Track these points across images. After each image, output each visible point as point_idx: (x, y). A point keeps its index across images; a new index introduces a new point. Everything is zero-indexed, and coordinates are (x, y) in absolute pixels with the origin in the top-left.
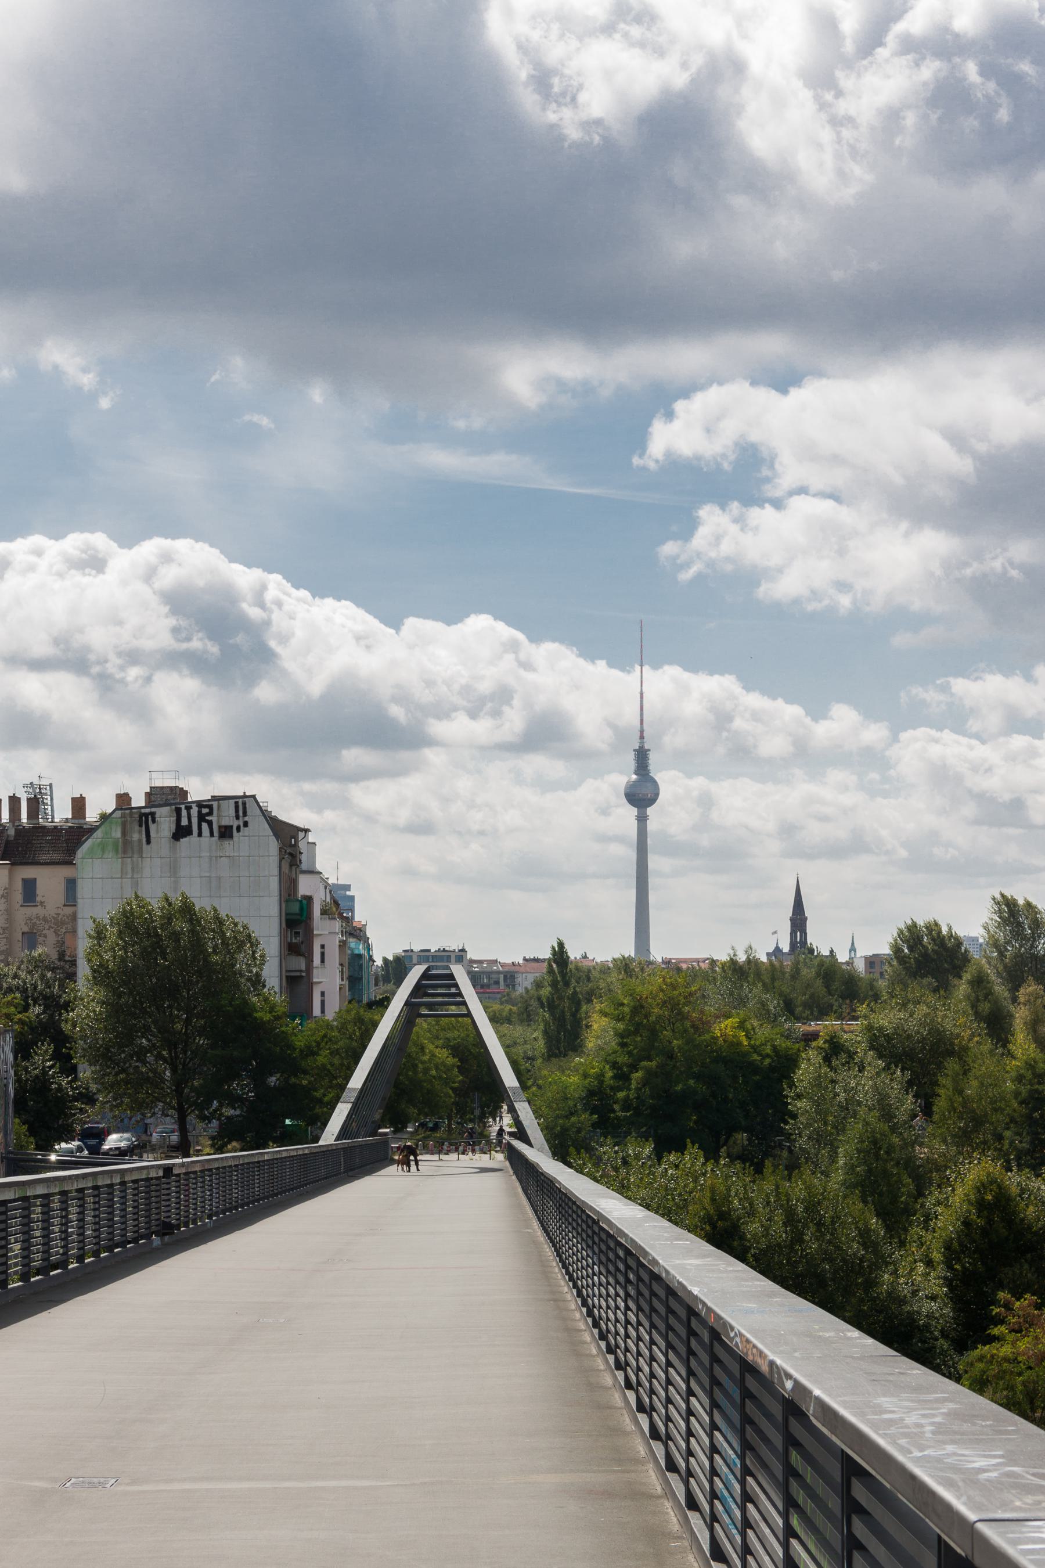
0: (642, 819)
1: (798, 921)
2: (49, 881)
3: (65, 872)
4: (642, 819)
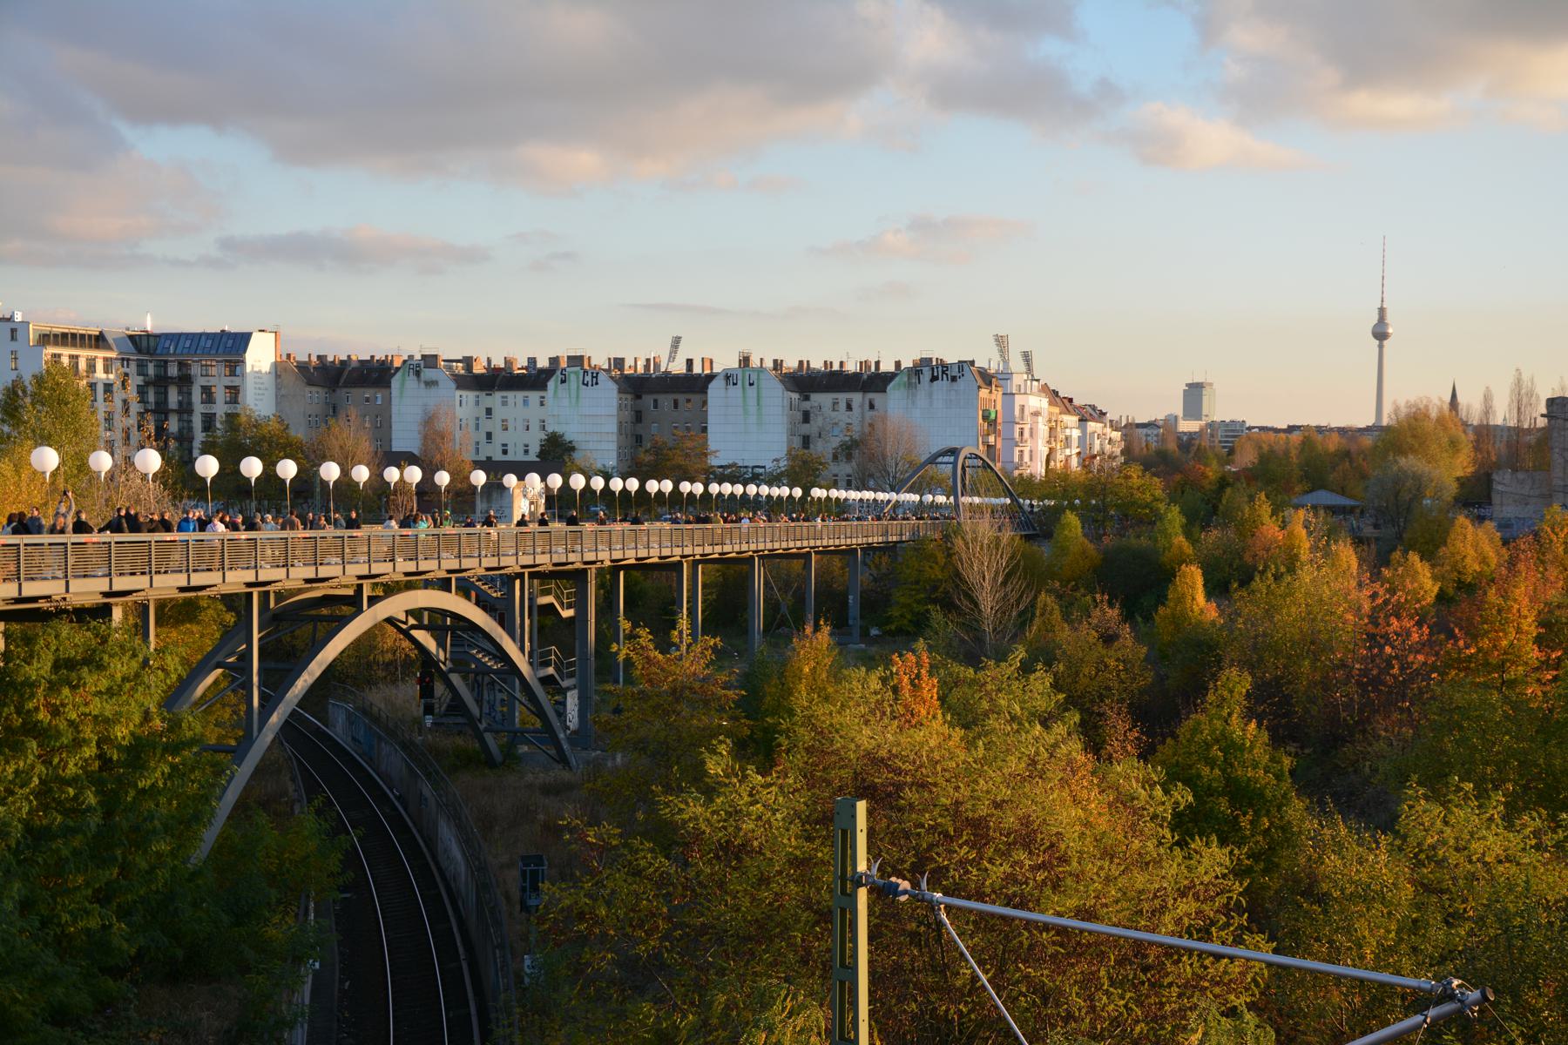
0: (1381, 347)
3: (385, 391)
4: (1381, 347)
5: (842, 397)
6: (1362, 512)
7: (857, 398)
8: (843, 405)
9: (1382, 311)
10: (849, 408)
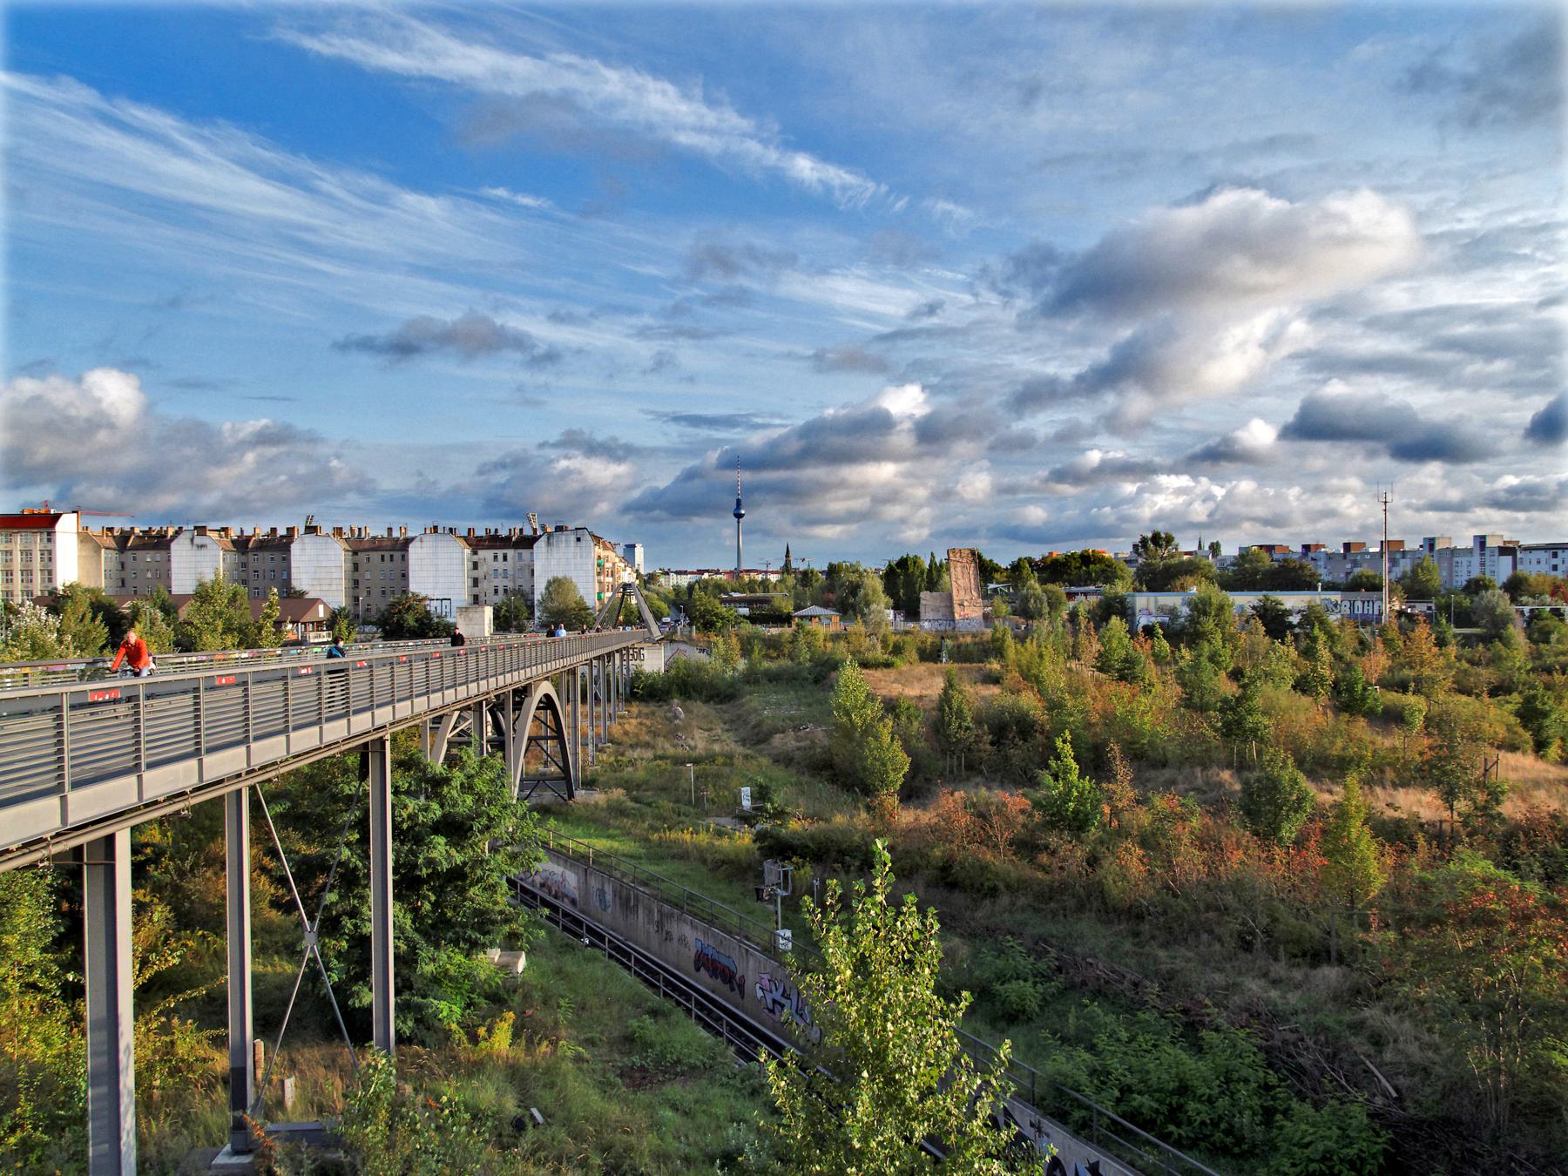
2: (525, 553)
5: (500, 553)
6: (496, 592)
7: (510, 553)
8: (500, 557)
9: (659, 416)
10: (505, 558)
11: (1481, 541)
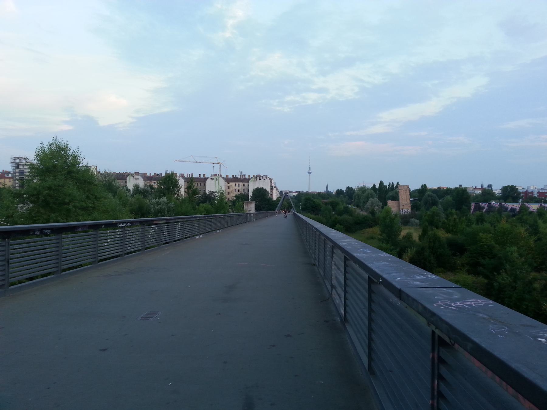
1: (327, 187)
2: (246, 184)
5: (237, 183)
7: (241, 184)
8: (237, 185)
11: (254, 176)
